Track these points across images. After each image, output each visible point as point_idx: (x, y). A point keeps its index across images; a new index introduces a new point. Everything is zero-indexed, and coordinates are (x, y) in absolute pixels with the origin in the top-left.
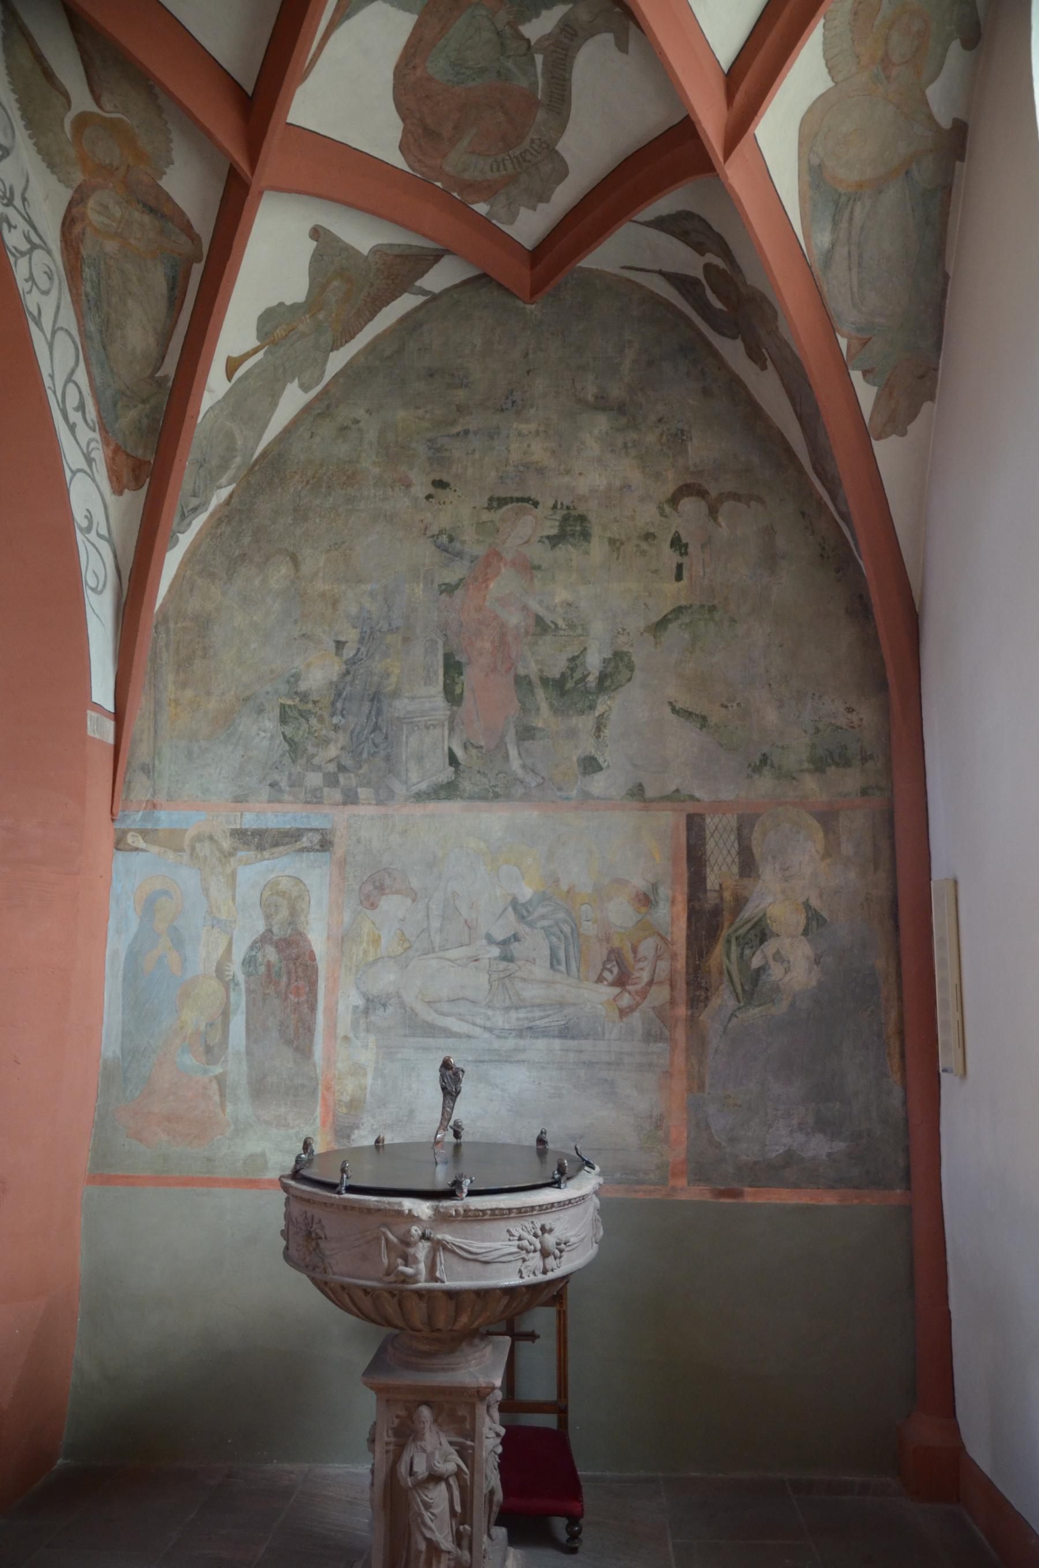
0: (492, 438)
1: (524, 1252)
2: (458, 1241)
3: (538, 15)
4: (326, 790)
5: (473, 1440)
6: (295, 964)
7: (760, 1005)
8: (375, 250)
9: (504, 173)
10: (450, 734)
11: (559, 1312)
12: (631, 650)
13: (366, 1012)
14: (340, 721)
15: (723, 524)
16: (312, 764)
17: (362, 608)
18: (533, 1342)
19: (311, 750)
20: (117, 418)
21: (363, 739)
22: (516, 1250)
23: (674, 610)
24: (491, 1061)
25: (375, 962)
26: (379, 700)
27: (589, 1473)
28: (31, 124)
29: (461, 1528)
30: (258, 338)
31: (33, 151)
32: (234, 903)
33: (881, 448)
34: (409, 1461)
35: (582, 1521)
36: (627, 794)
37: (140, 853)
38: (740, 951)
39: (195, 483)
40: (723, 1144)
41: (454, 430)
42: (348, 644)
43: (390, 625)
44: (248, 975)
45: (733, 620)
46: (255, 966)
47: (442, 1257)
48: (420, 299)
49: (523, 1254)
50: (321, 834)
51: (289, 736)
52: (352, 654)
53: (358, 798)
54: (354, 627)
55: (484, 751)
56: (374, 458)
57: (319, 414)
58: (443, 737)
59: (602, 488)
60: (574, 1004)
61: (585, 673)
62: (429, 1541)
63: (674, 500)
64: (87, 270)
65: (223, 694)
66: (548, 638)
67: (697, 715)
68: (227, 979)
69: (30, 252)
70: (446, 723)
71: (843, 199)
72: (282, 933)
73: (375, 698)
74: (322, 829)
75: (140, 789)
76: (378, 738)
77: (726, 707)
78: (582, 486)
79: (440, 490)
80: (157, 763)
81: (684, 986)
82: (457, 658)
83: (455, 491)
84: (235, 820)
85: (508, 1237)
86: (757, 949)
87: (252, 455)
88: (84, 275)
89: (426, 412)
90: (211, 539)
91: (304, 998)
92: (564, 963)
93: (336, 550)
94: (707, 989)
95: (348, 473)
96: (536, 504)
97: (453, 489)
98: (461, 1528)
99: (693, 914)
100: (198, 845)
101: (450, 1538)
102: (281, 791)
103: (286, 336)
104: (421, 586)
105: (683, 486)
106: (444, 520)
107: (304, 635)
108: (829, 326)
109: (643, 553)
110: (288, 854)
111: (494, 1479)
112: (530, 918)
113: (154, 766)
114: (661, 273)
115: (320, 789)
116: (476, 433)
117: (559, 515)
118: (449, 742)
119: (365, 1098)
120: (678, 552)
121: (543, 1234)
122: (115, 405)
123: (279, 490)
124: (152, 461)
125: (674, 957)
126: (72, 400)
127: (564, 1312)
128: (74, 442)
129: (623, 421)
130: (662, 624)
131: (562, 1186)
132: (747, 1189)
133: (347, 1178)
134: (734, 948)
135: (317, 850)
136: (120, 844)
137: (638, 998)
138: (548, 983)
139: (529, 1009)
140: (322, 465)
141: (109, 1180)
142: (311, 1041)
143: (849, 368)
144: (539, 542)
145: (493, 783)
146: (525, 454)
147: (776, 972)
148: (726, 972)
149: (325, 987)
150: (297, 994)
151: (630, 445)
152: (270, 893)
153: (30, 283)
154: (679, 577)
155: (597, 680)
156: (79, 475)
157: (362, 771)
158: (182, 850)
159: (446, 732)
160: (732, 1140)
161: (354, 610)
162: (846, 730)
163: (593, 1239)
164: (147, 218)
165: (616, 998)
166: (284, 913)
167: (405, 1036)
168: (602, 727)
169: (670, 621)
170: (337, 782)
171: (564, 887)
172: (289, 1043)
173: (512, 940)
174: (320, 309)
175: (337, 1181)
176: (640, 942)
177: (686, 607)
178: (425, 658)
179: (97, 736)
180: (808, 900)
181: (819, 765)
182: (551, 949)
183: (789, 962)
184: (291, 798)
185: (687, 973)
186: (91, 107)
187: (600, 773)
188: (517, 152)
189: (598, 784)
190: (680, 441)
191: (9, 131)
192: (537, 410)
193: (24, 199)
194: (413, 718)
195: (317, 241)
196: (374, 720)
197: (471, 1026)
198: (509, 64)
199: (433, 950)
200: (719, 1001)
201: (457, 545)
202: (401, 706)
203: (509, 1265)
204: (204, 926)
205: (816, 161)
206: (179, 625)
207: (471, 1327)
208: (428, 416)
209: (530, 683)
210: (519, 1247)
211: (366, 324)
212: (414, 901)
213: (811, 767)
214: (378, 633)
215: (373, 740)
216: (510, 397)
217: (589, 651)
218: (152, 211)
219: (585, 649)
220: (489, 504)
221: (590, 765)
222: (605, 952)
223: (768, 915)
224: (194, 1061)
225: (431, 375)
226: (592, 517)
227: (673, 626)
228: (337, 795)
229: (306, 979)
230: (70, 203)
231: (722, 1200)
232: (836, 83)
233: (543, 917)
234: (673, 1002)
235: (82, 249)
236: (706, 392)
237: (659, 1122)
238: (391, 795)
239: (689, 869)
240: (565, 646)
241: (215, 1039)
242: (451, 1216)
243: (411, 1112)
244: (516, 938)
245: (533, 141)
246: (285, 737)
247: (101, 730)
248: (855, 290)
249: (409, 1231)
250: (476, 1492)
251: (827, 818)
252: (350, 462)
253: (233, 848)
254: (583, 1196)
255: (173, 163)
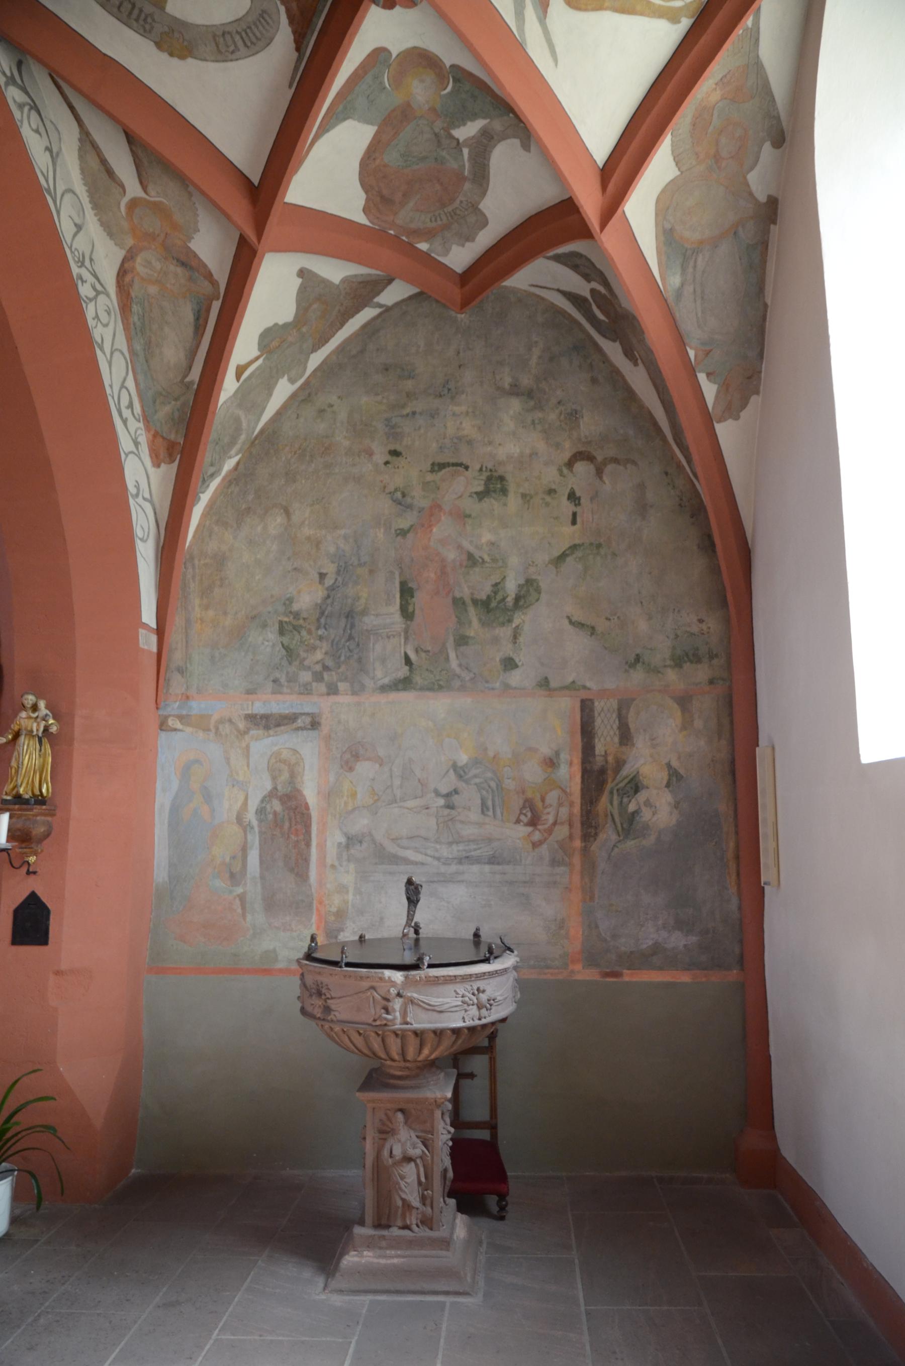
0: (433, 417)
1: (466, 1005)
2: (422, 998)
3: (464, 124)
4: (314, 684)
5: (432, 1135)
6: (294, 813)
7: (633, 839)
8: (344, 281)
9: (439, 222)
10: (405, 642)
11: (490, 1058)
12: (539, 578)
13: (347, 847)
14: (324, 633)
15: (607, 482)
16: (303, 665)
17: (338, 548)
18: (472, 1080)
19: (303, 654)
20: (156, 412)
21: (341, 646)
22: (460, 1003)
23: (570, 547)
24: (439, 881)
25: (354, 809)
26: (353, 617)
27: (513, 1174)
28: (96, 206)
29: (425, 1192)
30: (259, 349)
31: (100, 230)
32: (248, 769)
33: (721, 429)
34: (389, 1147)
35: (508, 1198)
36: (537, 685)
37: (178, 733)
38: (620, 800)
39: (212, 457)
40: (608, 939)
41: (405, 412)
42: (328, 576)
43: (359, 560)
44: (260, 821)
45: (614, 554)
46: (265, 814)
47: (410, 1008)
48: (377, 311)
49: (465, 1006)
50: (312, 717)
51: (286, 644)
52: (332, 582)
53: (338, 690)
54: (333, 562)
55: (431, 654)
56: (345, 433)
57: (303, 400)
58: (400, 644)
59: (516, 455)
60: (499, 840)
61: (505, 595)
62: (403, 1200)
63: (570, 464)
64: (135, 306)
65: (236, 613)
66: (477, 569)
67: (588, 626)
68: (245, 824)
69: (95, 298)
70: (402, 634)
71: (689, 253)
72: (285, 790)
73: (350, 615)
74: (312, 713)
75: (177, 685)
76: (352, 645)
77: (610, 620)
78: (502, 453)
79: (394, 458)
80: (188, 665)
81: (579, 825)
82: (410, 585)
83: (406, 458)
84: (248, 708)
85: (455, 995)
86: (633, 798)
87: (253, 433)
88: (133, 310)
89: (383, 397)
90: (224, 496)
91: (301, 837)
92: (491, 810)
93: (318, 504)
94: (596, 828)
95: (326, 445)
96: (467, 468)
97: (405, 457)
98: (425, 1192)
99: (586, 773)
100: (221, 727)
101: (418, 1199)
102: (281, 685)
103: (279, 346)
104: (382, 530)
105: (577, 452)
106: (398, 481)
107: (295, 569)
108: (681, 341)
109: (547, 504)
110: (288, 732)
111: (448, 1162)
112: (467, 777)
113: (186, 668)
114: (558, 290)
115: (311, 683)
116: (421, 414)
117: (485, 475)
118: (405, 648)
119: (348, 909)
120: (573, 503)
121: (478, 993)
122: (154, 402)
123: (274, 459)
124: (182, 443)
125: (572, 804)
126: (125, 402)
127: (494, 1058)
128: (126, 432)
129: (532, 403)
130: (562, 557)
131: (491, 962)
132: (625, 971)
133: (346, 957)
134: (615, 797)
135: (309, 729)
136: (163, 725)
137: (546, 835)
138: (480, 825)
139: (466, 843)
140: (305, 439)
141: (162, 971)
142: (308, 868)
143: (697, 371)
144: (469, 496)
145: (438, 678)
146: (458, 429)
147: (646, 815)
148: (609, 814)
149: (317, 829)
150: (297, 835)
151: (537, 421)
152: (274, 761)
153: (96, 320)
154: (574, 522)
155: (514, 601)
156: (131, 456)
157: (341, 670)
158: (209, 730)
159: (403, 641)
160: (615, 937)
161: (332, 549)
162: (698, 635)
163: (513, 1000)
164: (179, 270)
165: (529, 835)
166: (285, 776)
167: (376, 864)
168: (518, 635)
169: (567, 555)
170: (323, 678)
171: (491, 754)
172: (292, 870)
173: (453, 793)
174: (305, 324)
175: (339, 960)
176: (546, 793)
177: (579, 545)
178: (386, 585)
179: (146, 647)
180: (670, 761)
181: (678, 662)
182: (482, 799)
183: (656, 807)
184: (289, 691)
185: (582, 816)
186: (141, 194)
187: (517, 669)
188: (450, 209)
189: (515, 678)
190: (574, 418)
191: (81, 213)
192: (467, 395)
193: (91, 260)
194: (378, 630)
195: (302, 278)
196: (349, 632)
197: (424, 856)
198: (444, 153)
199: (396, 802)
200: (605, 836)
201: (408, 500)
202: (369, 621)
203: (456, 1013)
204: (227, 785)
205: (668, 226)
206: (202, 562)
207: (429, 1059)
208: (385, 401)
209: (464, 603)
210: (462, 1002)
211: (337, 331)
212: (381, 765)
213: (672, 663)
214: (351, 567)
215: (348, 647)
216: (447, 386)
217: (508, 579)
218: (183, 264)
219: (505, 577)
220: (432, 468)
221: (509, 664)
222: (521, 802)
223: (640, 773)
224: (222, 884)
225: (387, 370)
226: (509, 477)
227: (569, 559)
228: (323, 688)
229: (303, 824)
230: (123, 260)
231: (609, 979)
232: (682, 173)
233: (475, 776)
234: (571, 837)
235: (131, 290)
236: (594, 381)
237: (561, 925)
238: (363, 687)
239: (582, 740)
240: (490, 575)
241: (237, 868)
242: (417, 981)
243: (382, 919)
244: (456, 792)
245: (461, 202)
246: (283, 645)
247: (148, 642)
248: (700, 314)
249: (389, 991)
250: (435, 1169)
251: (684, 701)
252: (327, 437)
253: (247, 728)
254: (505, 969)
255: (199, 231)
